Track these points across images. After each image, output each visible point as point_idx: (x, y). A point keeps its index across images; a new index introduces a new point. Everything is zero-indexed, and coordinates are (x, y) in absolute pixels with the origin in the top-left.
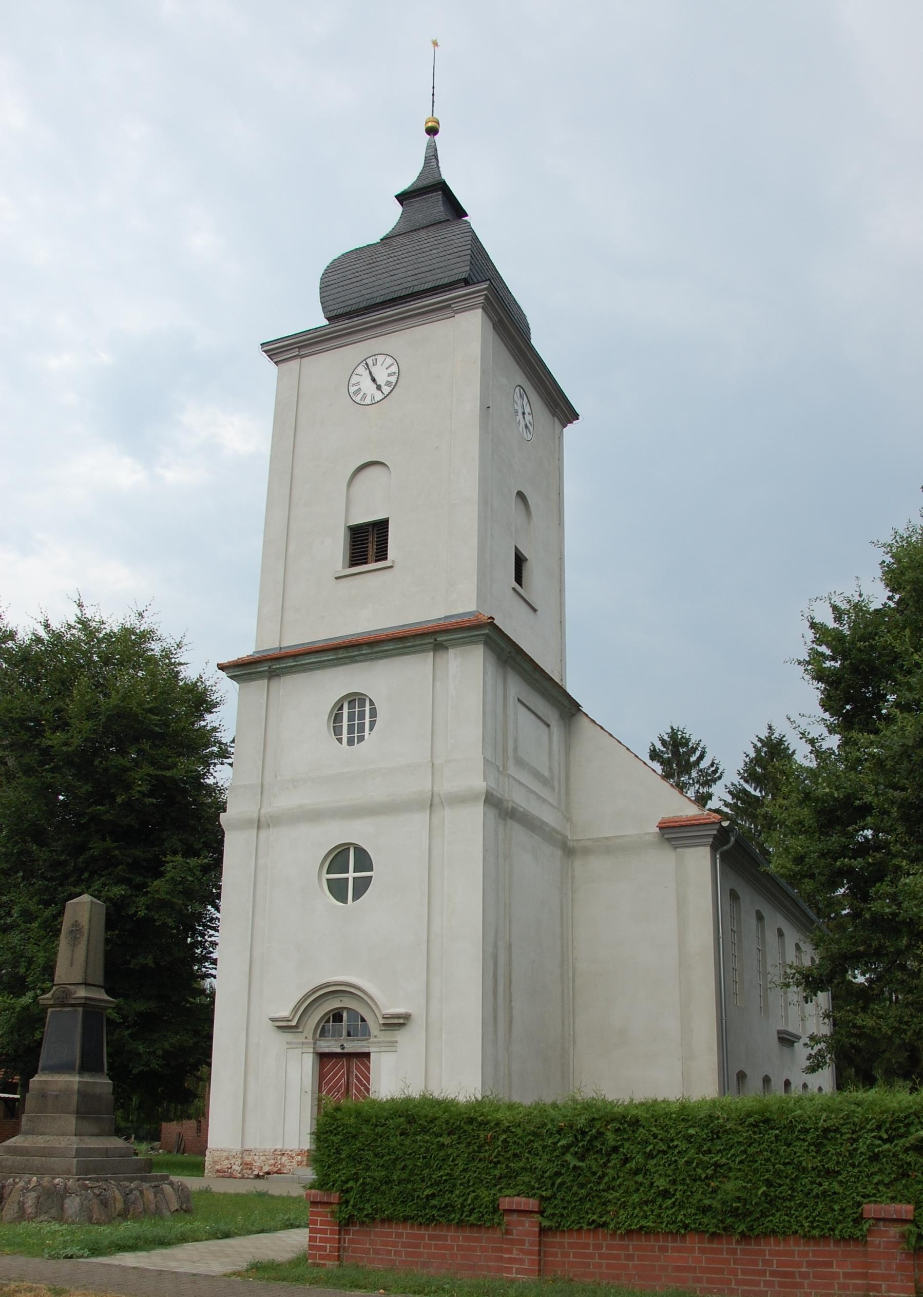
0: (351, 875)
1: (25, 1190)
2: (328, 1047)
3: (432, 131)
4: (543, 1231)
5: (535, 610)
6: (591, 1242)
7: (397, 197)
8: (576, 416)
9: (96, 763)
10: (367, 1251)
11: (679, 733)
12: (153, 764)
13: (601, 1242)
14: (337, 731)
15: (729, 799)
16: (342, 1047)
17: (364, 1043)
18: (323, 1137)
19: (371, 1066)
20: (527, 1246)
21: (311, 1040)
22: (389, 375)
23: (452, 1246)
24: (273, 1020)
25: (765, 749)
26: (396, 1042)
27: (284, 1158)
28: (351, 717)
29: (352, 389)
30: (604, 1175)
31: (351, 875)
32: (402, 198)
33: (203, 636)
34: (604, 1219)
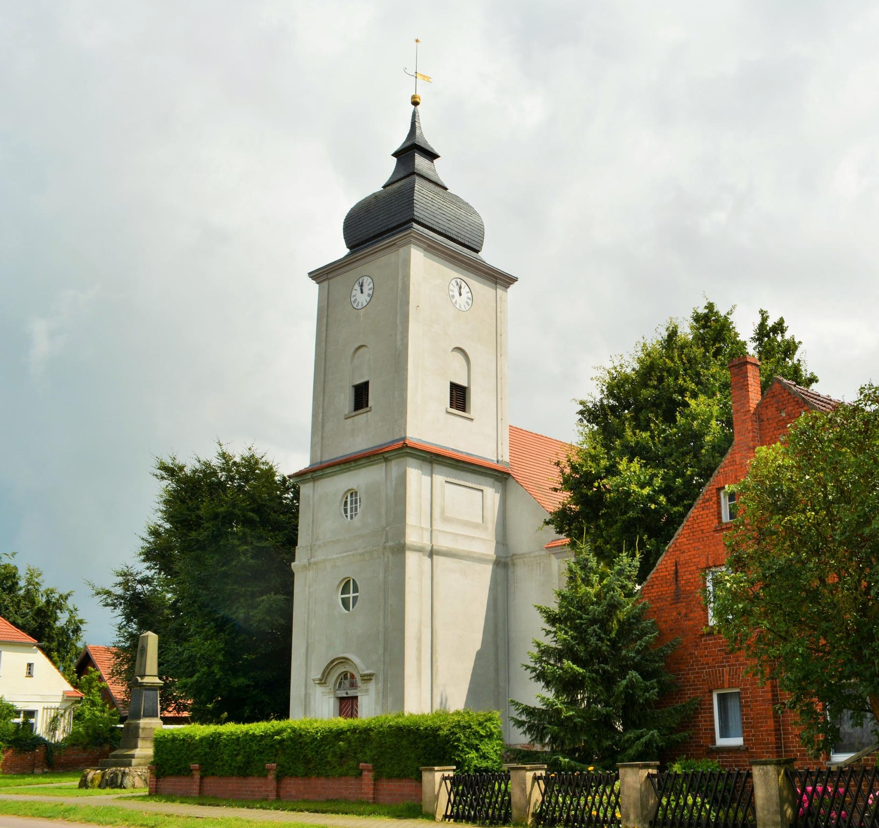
15: (147, 564)
32: (395, 155)
33: (289, 459)
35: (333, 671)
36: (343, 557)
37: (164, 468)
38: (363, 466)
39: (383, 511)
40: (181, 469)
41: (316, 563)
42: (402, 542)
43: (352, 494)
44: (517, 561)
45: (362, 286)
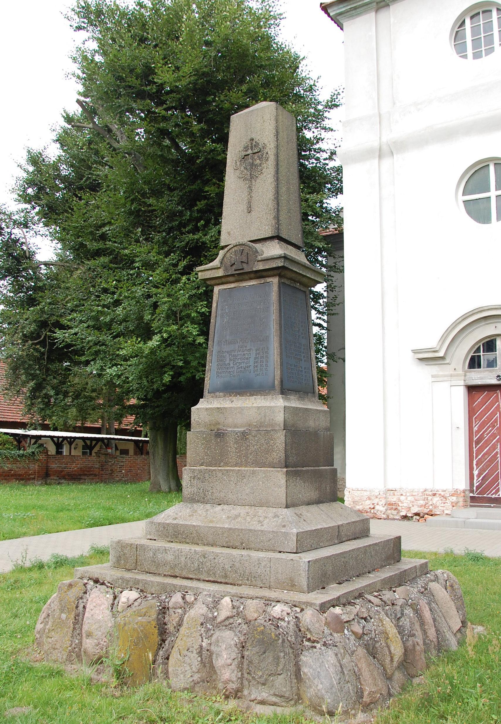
1: (210, 624)
21: (461, 372)
24: (415, 352)
27: (436, 499)
28: (475, 31)
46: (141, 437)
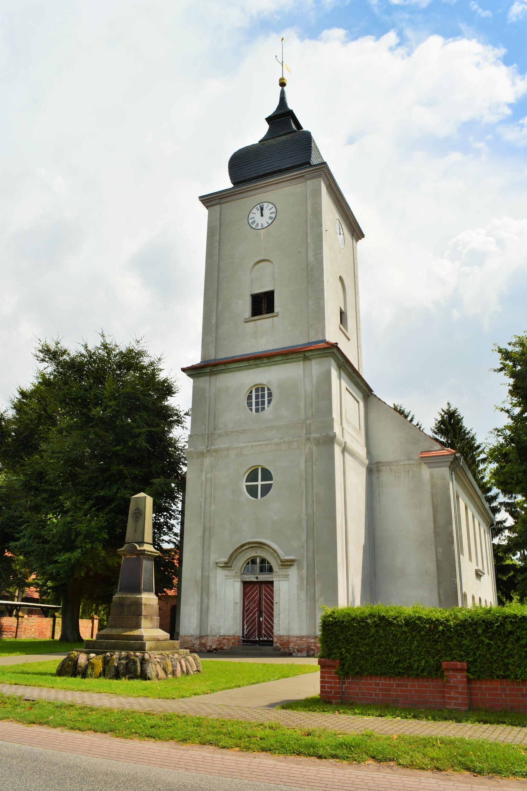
0: (260, 483)
2: (269, 578)
3: (283, 84)
4: (469, 680)
5: (349, 340)
6: (499, 687)
7: (267, 119)
8: (363, 236)
9: (117, 423)
10: (357, 694)
11: (399, 407)
12: (148, 425)
13: (521, 687)
14: (250, 405)
16: (257, 578)
17: (270, 576)
18: (327, 628)
19: (275, 589)
20: (460, 690)
22: (271, 213)
23: (411, 691)
25: (446, 416)
26: (289, 575)
28: (257, 397)
29: (250, 221)
30: (506, 647)
31: (260, 483)
34: (507, 673)
35: (240, 556)
36: (252, 446)
37: (46, 351)
38: (276, 363)
39: (302, 405)
40: (64, 352)
41: (216, 451)
42: (331, 434)
43: (257, 390)
44: (384, 468)
45: (262, 209)
46: (14, 601)
